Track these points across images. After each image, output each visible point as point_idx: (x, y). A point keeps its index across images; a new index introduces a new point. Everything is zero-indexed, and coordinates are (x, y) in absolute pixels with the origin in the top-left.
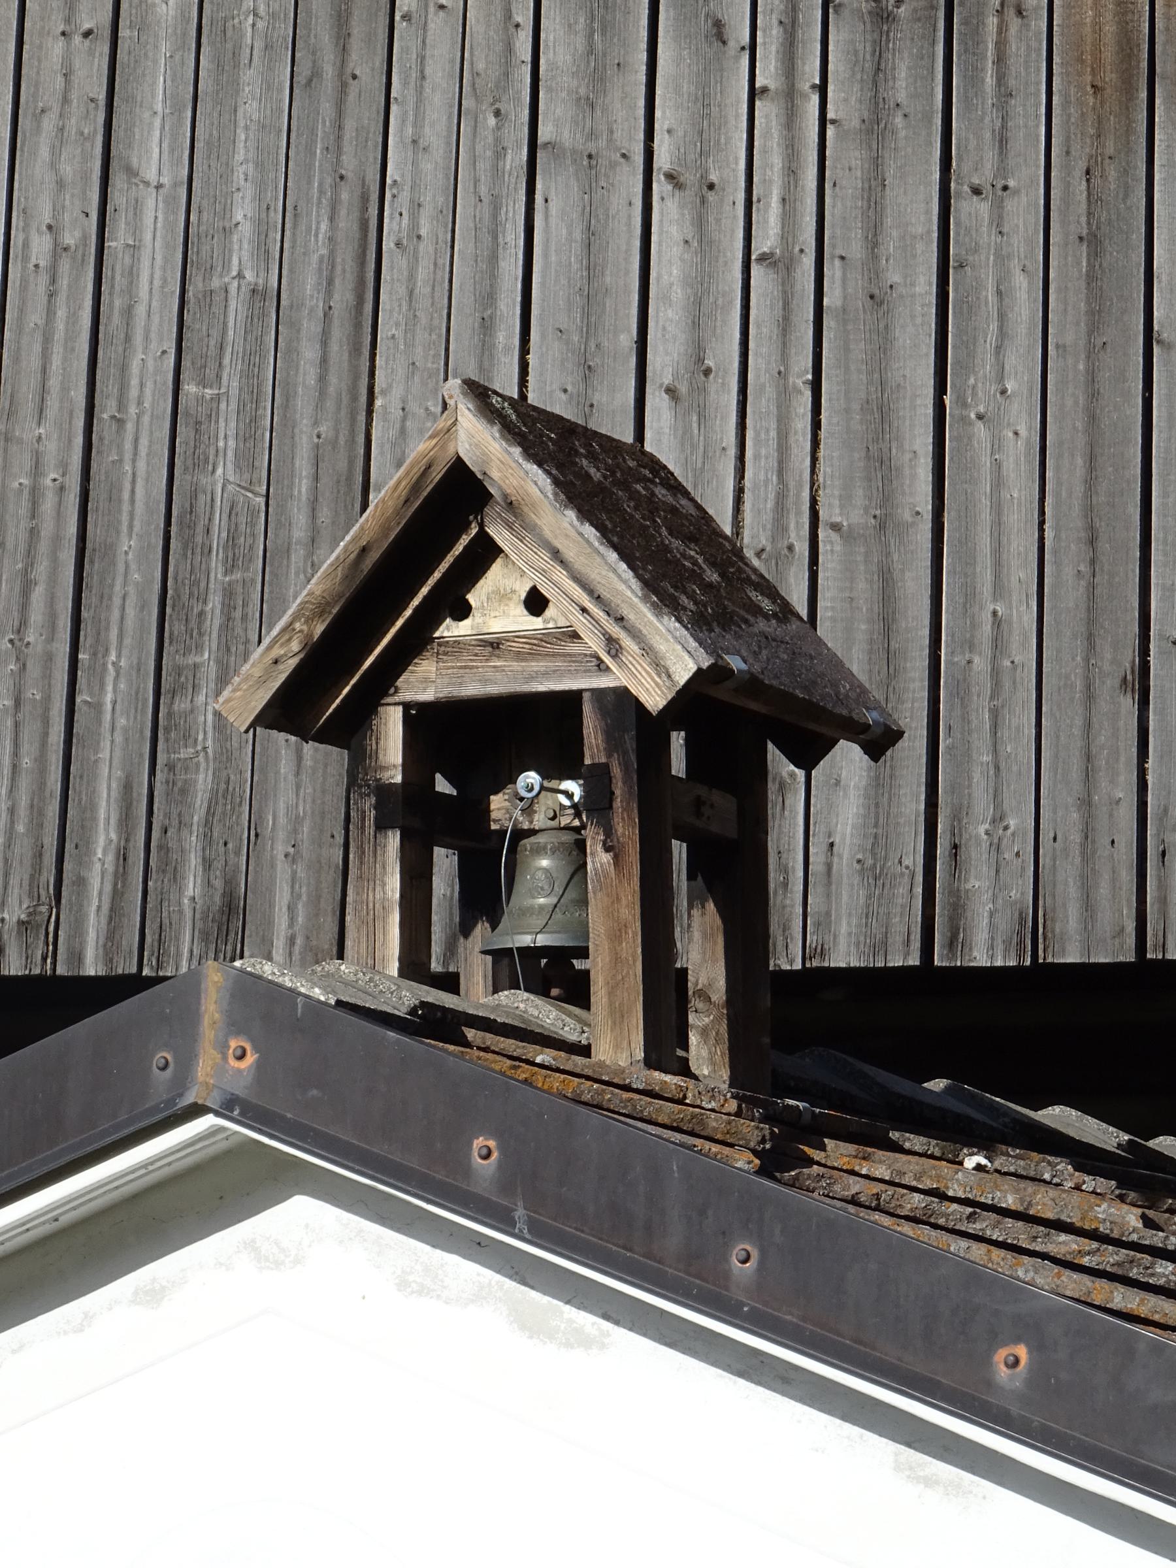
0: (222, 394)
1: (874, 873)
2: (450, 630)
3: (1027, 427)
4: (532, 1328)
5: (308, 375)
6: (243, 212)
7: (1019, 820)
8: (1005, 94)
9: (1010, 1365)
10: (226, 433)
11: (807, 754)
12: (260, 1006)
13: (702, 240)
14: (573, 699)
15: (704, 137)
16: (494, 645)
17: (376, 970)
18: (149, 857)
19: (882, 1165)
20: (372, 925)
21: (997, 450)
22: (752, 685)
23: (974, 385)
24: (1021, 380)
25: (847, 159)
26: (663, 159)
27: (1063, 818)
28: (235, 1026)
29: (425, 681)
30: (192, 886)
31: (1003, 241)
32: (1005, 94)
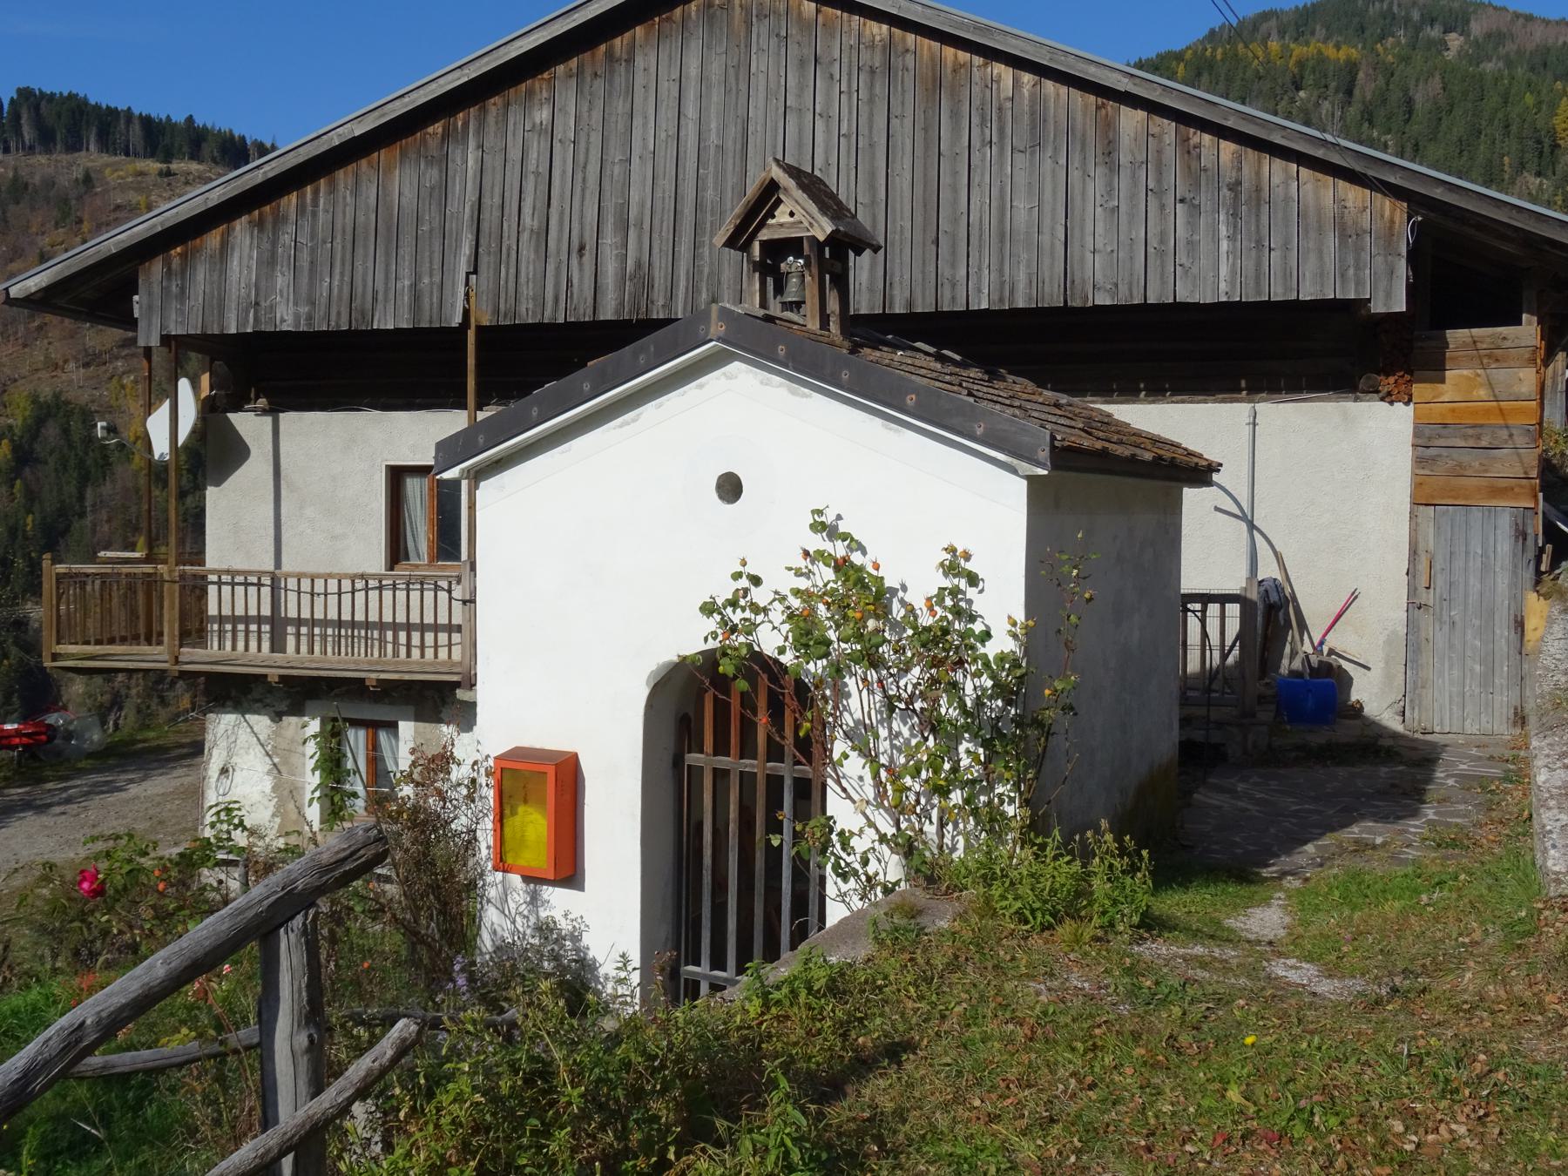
0: (709, 172)
1: (871, 290)
2: (771, 221)
3: (909, 177)
4: (794, 393)
5: (730, 167)
6: (713, 125)
7: (907, 277)
8: (903, 91)
9: (911, 400)
10: (710, 182)
11: (858, 253)
12: (726, 314)
13: (828, 131)
14: (801, 238)
15: (828, 104)
16: (781, 225)
17: (753, 304)
18: (693, 289)
19: (878, 354)
20: (752, 295)
21: (902, 183)
22: (846, 235)
23: (896, 167)
24: (907, 165)
25: (864, 109)
27: (917, 276)
29: (764, 235)
30: (704, 296)
31: (903, 130)
32: (903, 91)
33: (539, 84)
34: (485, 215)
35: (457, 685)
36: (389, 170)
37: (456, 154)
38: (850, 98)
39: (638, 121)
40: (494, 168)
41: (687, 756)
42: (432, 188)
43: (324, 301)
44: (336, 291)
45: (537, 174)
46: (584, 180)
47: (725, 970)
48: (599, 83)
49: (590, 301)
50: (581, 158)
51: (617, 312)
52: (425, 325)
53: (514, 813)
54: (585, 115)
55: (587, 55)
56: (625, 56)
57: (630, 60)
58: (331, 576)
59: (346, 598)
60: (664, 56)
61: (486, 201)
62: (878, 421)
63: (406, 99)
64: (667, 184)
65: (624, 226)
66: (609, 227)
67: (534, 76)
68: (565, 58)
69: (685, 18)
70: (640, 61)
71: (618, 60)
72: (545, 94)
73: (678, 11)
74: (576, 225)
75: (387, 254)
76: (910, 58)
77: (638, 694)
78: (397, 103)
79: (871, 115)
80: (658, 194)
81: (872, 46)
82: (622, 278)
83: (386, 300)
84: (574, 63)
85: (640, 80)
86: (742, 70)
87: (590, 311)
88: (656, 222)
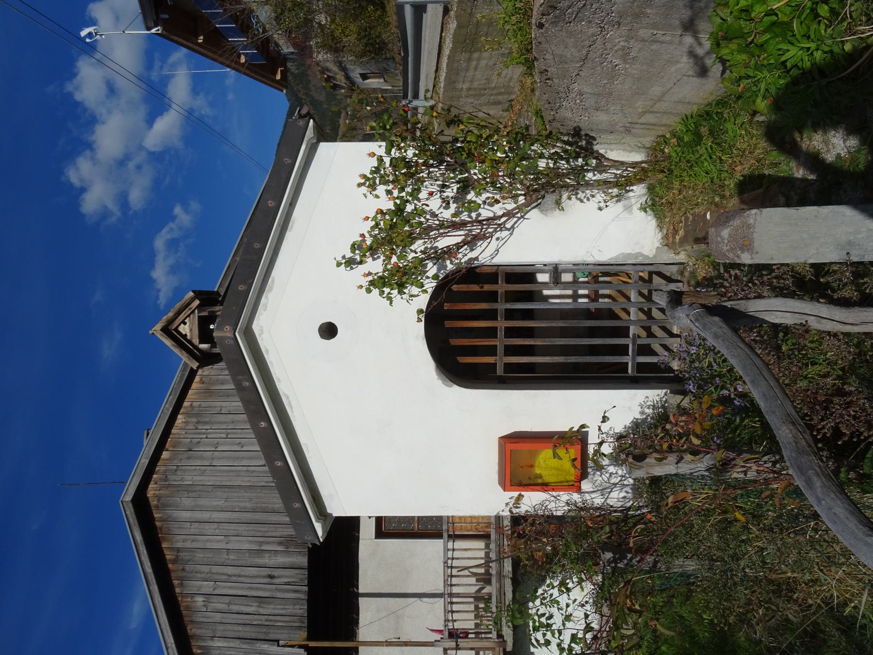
2: (188, 337)
4: (271, 289)
5: (236, 494)
10: (242, 505)
13: (224, 444)
16: (191, 330)
26: (213, 449)
28: (223, 330)
29: (196, 341)
33: (184, 602)
34: (248, 635)
35: (504, 650)
38: (210, 433)
39: (209, 545)
40: (224, 630)
45: (229, 604)
46: (235, 576)
47: (627, 363)
48: (187, 567)
49: (297, 571)
50: (224, 577)
51: (304, 555)
53: (540, 476)
54: (202, 575)
56: (175, 553)
57: (178, 550)
61: (241, 635)
62: (289, 236)
64: (242, 528)
65: (260, 552)
66: (260, 561)
68: (172, 587)
69: (162, 520)
70: (179, 545)
71: (177, 556)
72: (189, 599)
73: (157, 524)
74: (257, 580)
76: (195, 404)
77: (457, 391)
79: (219, 423)
82: (286, 553)
84: (176, 582)
85: (188, 545)
86: (189, 489)
87: (303, 572)
88: (259, 534)
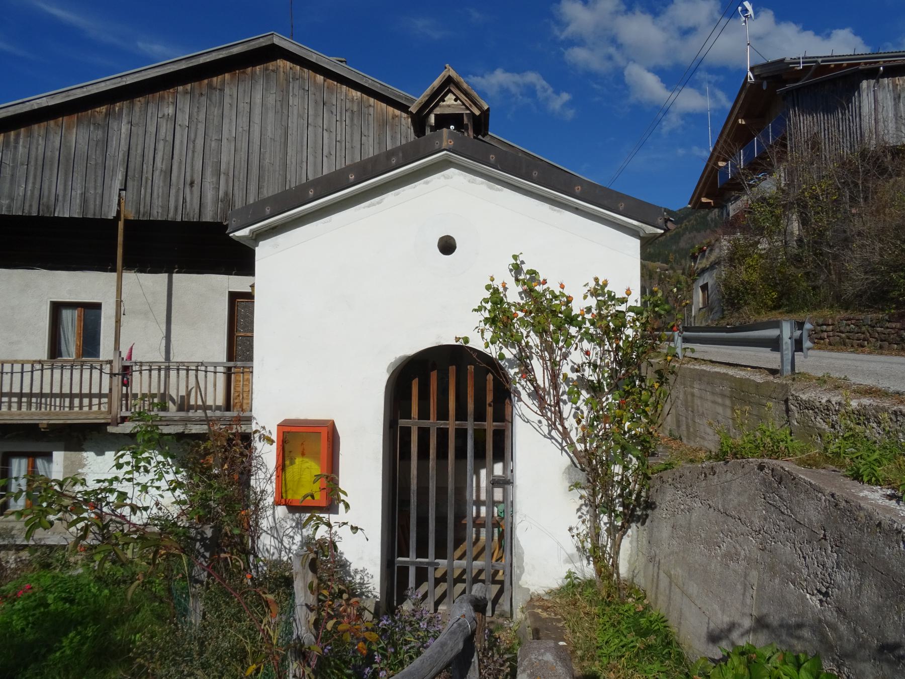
2: (441, 103)
4: (491, 188)
13: (330, 138)
29: (438, 111)
33: (168, 94)
34: (132, 159)
35: (109, 424)
36: (69, 128)
37: (114, 125)
38: (341, 125)
41: (400, 421)
42: (98, 142)
43: (20, 198)
44: (29, 193)
45: (165, 140)
47: (427, 558)
48: (204, 99)
49: (197, 211)
50: (192, 136)
51: (213, 218)
52: (90, 216)
53: (292, 463)
55: (197, 83)
57: (222, 90)
58: (16, 362)
59: (27, 377)
60: (241, 90)
61: (132, 152)
62: (545, 207)
63: (85, 89)
67: (164, 90)
68: (184, 83)
71: (215, 89)
72: (170, 100)
73: (249, 69)
74: (188, 169)
75: (66, 174)
76: (371, 109)
78: (78, 90)
80: (237, 159)
81: (352, 101)
82: (217, 200)
83: (64, 200)
84: (189, 87)
85: (227, 100)
86: (284, 102)
87: (197, 216)
88: (236, 173)
